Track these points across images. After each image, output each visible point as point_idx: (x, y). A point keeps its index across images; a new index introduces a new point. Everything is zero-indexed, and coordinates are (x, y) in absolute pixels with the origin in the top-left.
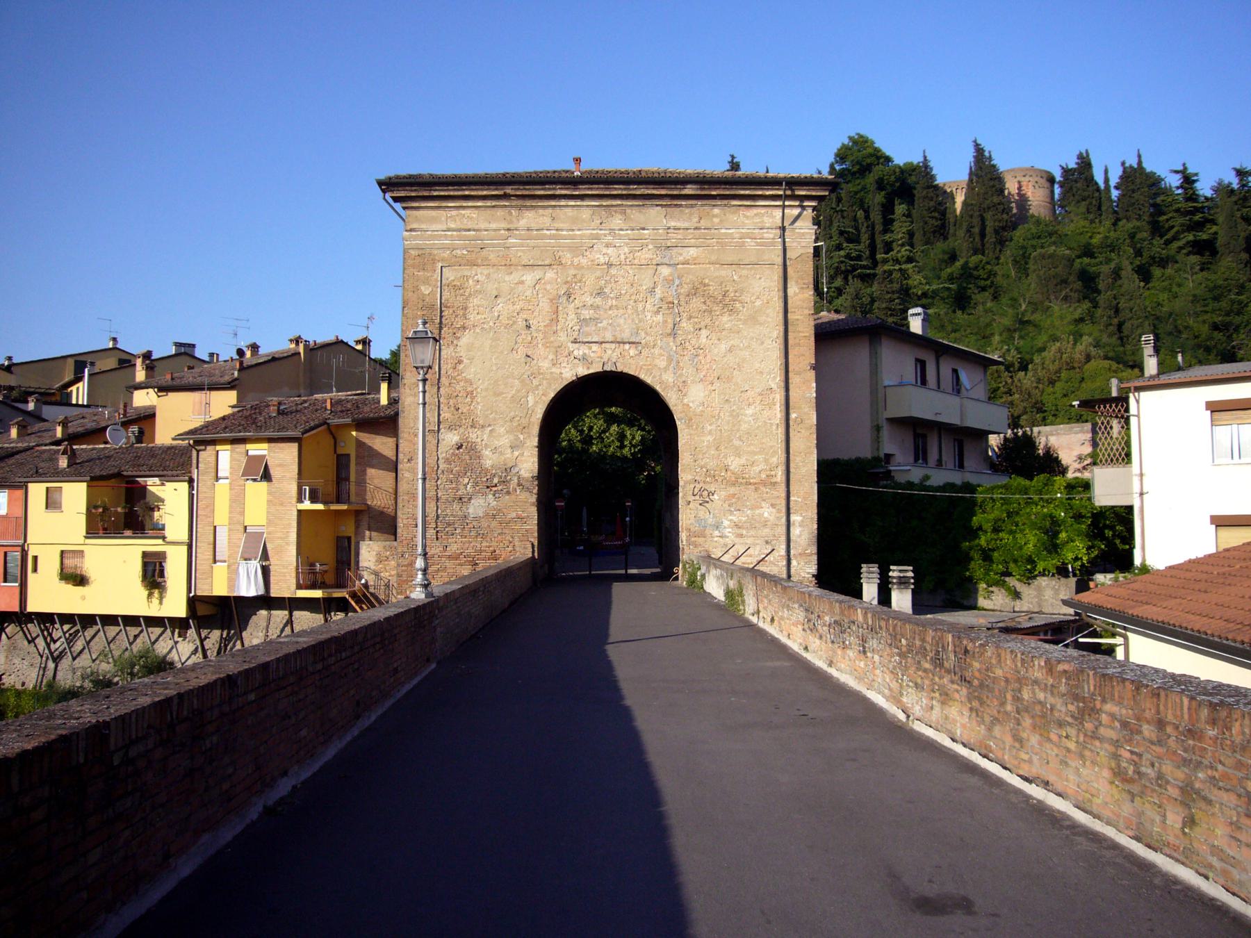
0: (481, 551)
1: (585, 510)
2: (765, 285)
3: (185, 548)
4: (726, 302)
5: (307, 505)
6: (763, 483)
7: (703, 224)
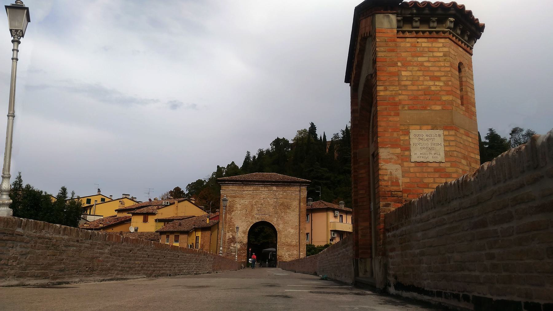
2: (295, 203)
6: (295, 246)
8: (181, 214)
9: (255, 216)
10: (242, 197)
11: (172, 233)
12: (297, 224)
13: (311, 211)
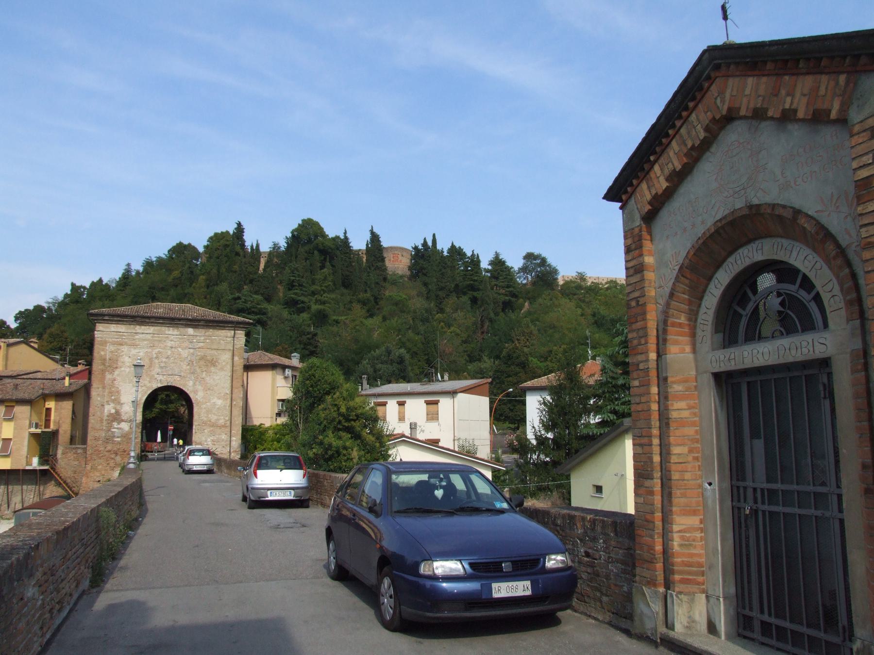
2: (226, 357)
4: (213, 363)
6: (223, 426)
12: (228, 392)
13: (249, 368)
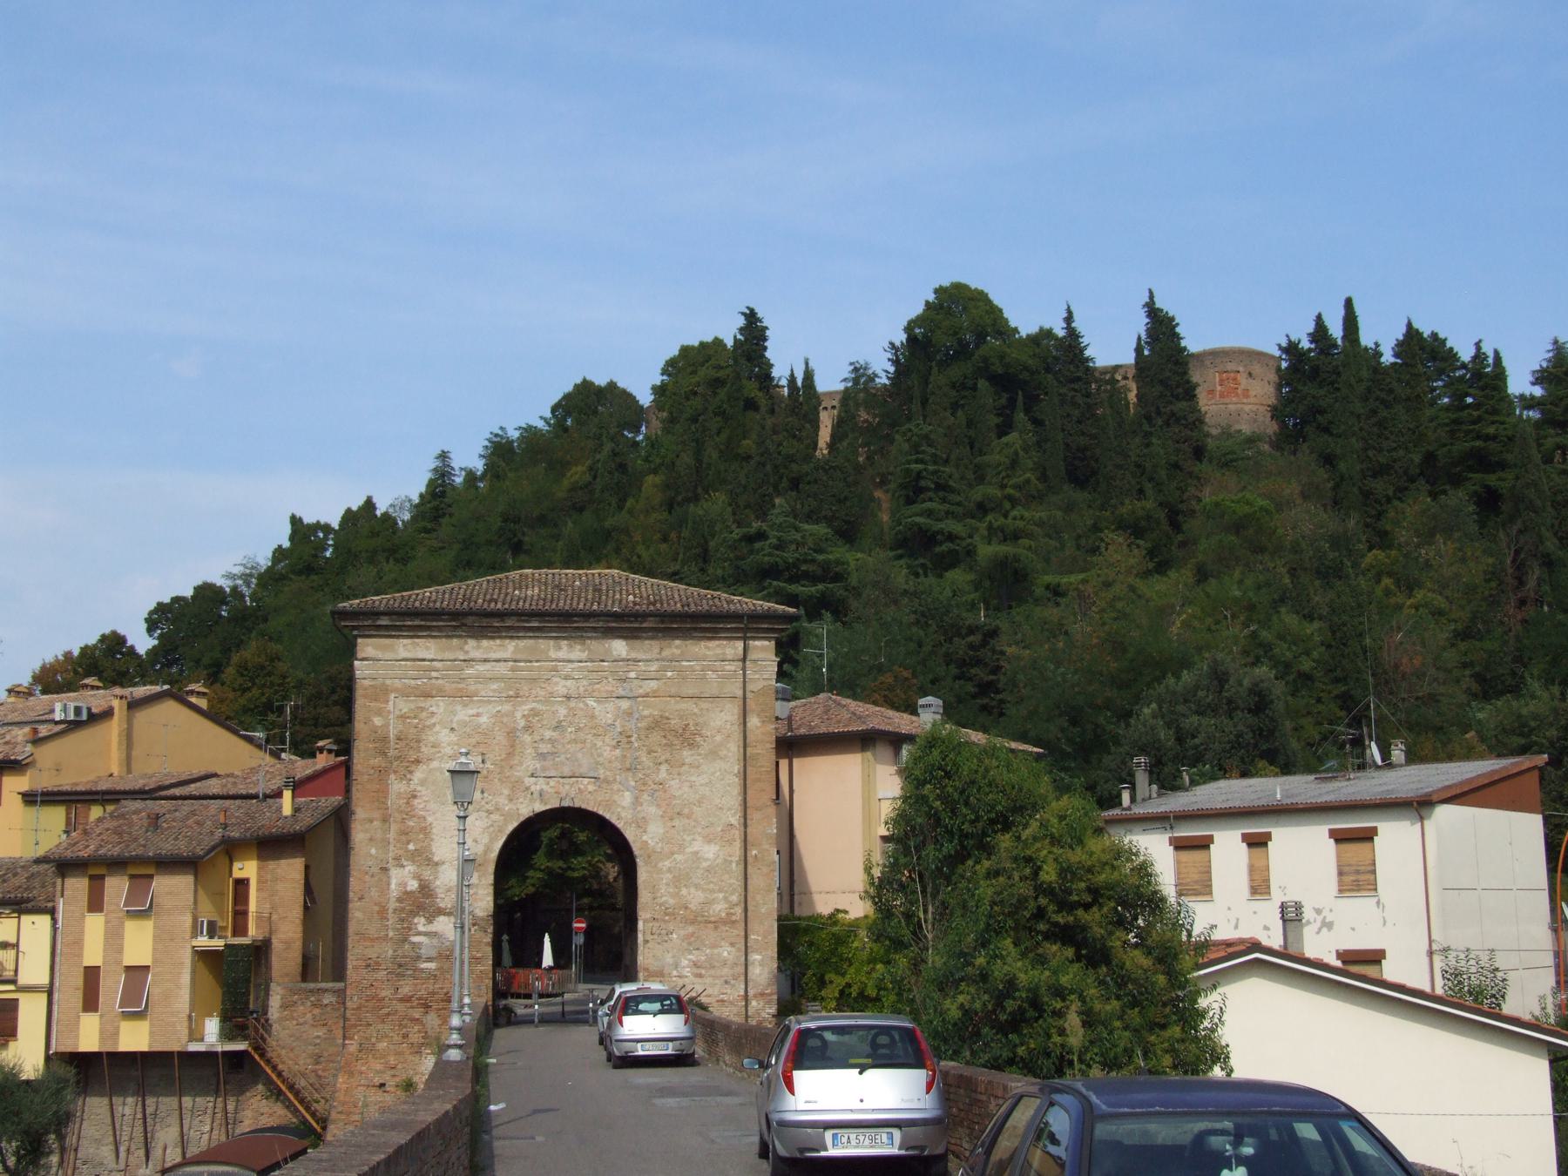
0: (434, 993)
1: (547, 939)
2: (724, 718)
3: (45, 996)
4: (687, 736)
5: (203, 941)
6: (724, 922)
7: (665, 654)
8: (154, 767)
9: (529, 781)
10: (465, 696)
11: (117, 864)
